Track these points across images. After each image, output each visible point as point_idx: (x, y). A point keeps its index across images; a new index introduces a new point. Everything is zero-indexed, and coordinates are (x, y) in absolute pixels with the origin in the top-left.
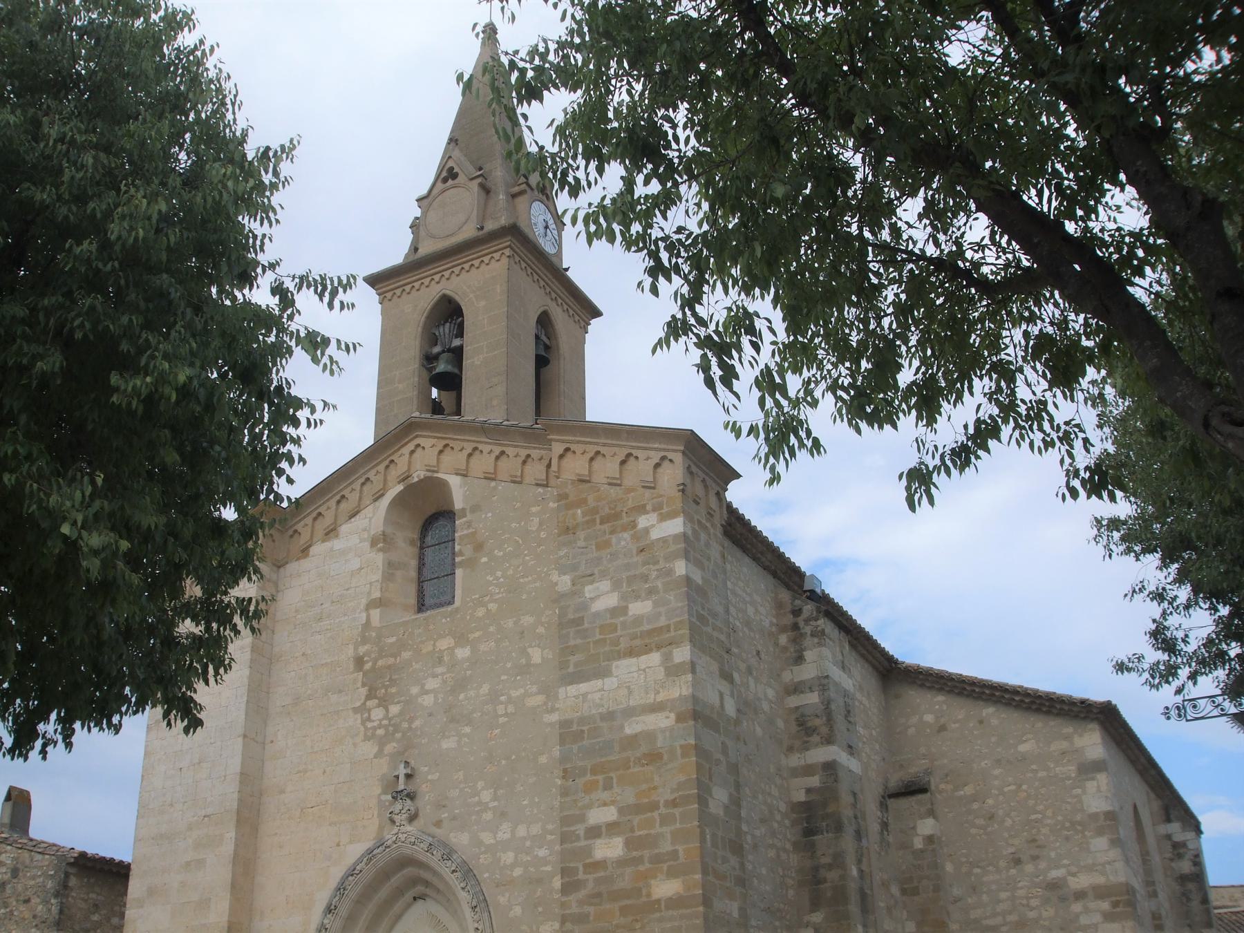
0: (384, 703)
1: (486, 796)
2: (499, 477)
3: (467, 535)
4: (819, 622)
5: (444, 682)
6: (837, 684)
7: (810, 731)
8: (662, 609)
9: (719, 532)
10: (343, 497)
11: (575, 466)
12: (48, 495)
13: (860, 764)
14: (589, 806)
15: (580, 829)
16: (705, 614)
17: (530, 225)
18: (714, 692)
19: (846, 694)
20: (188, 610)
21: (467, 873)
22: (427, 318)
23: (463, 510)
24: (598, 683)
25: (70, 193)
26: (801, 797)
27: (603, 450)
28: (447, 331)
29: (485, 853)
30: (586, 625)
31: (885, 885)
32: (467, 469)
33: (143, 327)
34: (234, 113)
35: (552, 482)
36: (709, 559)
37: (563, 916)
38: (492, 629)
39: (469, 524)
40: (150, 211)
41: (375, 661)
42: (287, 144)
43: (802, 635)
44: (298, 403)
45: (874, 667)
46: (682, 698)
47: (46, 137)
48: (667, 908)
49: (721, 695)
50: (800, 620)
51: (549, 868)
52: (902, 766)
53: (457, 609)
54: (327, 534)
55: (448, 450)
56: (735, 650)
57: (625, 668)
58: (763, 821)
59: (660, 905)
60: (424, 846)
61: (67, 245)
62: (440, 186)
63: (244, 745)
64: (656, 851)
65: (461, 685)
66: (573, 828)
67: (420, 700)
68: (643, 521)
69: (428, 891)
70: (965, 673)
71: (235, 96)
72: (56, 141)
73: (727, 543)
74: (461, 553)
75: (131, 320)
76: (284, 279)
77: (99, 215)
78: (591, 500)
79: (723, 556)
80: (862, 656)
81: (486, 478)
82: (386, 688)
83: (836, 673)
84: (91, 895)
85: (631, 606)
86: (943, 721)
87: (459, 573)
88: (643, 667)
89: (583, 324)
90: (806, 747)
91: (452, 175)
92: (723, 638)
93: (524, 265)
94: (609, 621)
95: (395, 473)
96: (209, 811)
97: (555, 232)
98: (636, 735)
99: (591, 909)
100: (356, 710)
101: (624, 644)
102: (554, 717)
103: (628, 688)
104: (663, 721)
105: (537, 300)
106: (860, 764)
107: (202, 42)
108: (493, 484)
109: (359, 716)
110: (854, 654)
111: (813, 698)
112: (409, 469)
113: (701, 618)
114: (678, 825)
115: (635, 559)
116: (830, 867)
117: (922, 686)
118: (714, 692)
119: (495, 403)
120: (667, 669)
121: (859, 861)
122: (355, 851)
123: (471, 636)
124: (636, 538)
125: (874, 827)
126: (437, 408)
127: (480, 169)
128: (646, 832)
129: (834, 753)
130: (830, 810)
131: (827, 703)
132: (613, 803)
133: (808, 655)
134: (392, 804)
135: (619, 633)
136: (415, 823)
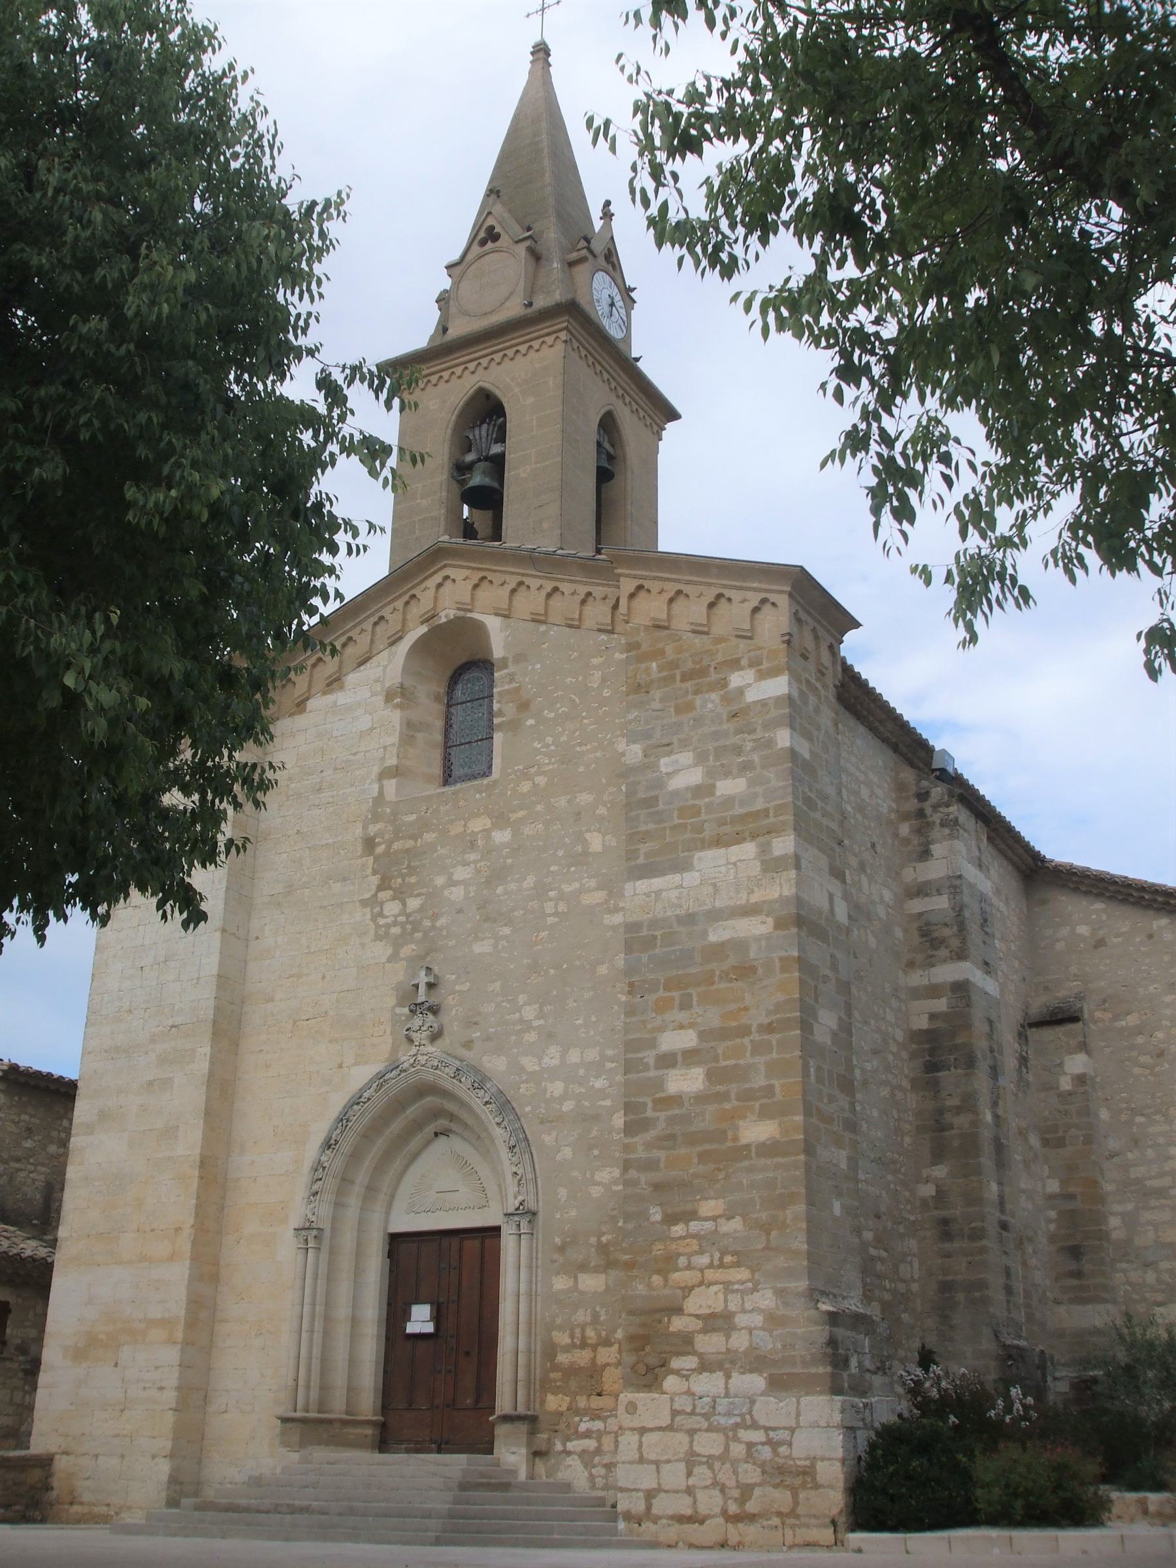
0: (400, 895)
1: (529, 1012)
2: (550, 620)
3: (508, 692)
4: (951, 809)
5: (478, 871)
6: (972, 886)
7: (936, 943)
8: (759, 789)
9: (831, 694)
10: (350, 639)
11: (651, 608)
12: (49, 635)
13: (997, 987)
14: (661, 1029)
15: (649, 1056)
16: (813, 796)
17: (591, 302)
18: (822, 893)
19: (983, 899)
20: (175, 779)
21: (504, 1105)
22: (459, 416)
23: (504, 659)
24: (676, 878)
25: (74, 257)
26: (922, 1023)
27: (686, 589)
28: (484, 434)
29: (526, 1081)
30: (661, 807)
31: (1022, 1134)
32: (509, 609)
33: (164, 426)
34: (272, 157)
35: (618, 629)
36: (818, 729)
37: (626, 1161)
38: (539, 808)
39: (512, 678)
40: (177, 281)
41: (390, 844)
42: (334, 198)
43: (930, 825)
44: (333, 525)
45: (1014, 864)
46: (782, 900)
47: (44, 185)
48: (760, 1154)
49: (831, 897)
50: (927, 806)
51: (608, 1103)
52: (1046, 988)
53: (496, 782)
54: (328, 685)
55: (485, 584)
56: (846, 842)
57: (710, 861)
58: (875, 1052)
59: (750, 1150)
60: (450, 1071)
61: (71, 323)
62: (476, 249)
63: (224, 941)
64: (747, 1086)
65: (497, 876)
66: (640, 1055)
67: (446, 893)
68: (736, 680)
69: (453, 1126)
70: (1131, 875)
71: (274, 137)
72: (57, 191)
73: (842, 710)
74: (501, 713)
75: (150, 418)
76: (331, 369)
77: (110, 286)
78: (669, 650)
79: (836, 725)
80: (1001, 851)
81: (533, 620)
82: (403, 877)
83: (971, 873)
84: (24, 1117)
85: (719, 784)
86: (1101, 933)
87: (498, 737)
88: (733, 859)
89: (656, 428)
90: (930, 963)
91: (492, 236)
92: (834, 826)
93: (584, 353)
94: (691, 802)
95: (416, 611)
96: (178, 1020)
97: (623, 311)
98: (723, 944)
99: (662, 1154)
100: (364, 903)
101: (709, 831)
102: (617, 919)
103: (714, 885)
104: (757, 927)
105: (599, 397)
106: (997, 987)
107: (231, 67)
108: (543, 628)
109: (368, 910)
110: (990, 849)
111: (941, 903)
112: (434, 608)
113: (808, 801)
114: (774, 1055)
115: (725, 727)
116: (958, 1110)
117: (1076, 890)
118: (822, 893)
119: (545, 525)
120: (763, 862)
121: (995, 1104)
122: (361, 1075)
123: (513, 817)
124: (727, 699)
125: (1010, 1062)
126: (469, 531)
127: (529, 229)
128: (733, 1062)
129: (967, 971)
130: (959, 1041)
131: (959, 910)
132: (692, 1025)
133: (937, 849)
134: (409, 1019)
135: (703, 817)
136: (439, 1042)
